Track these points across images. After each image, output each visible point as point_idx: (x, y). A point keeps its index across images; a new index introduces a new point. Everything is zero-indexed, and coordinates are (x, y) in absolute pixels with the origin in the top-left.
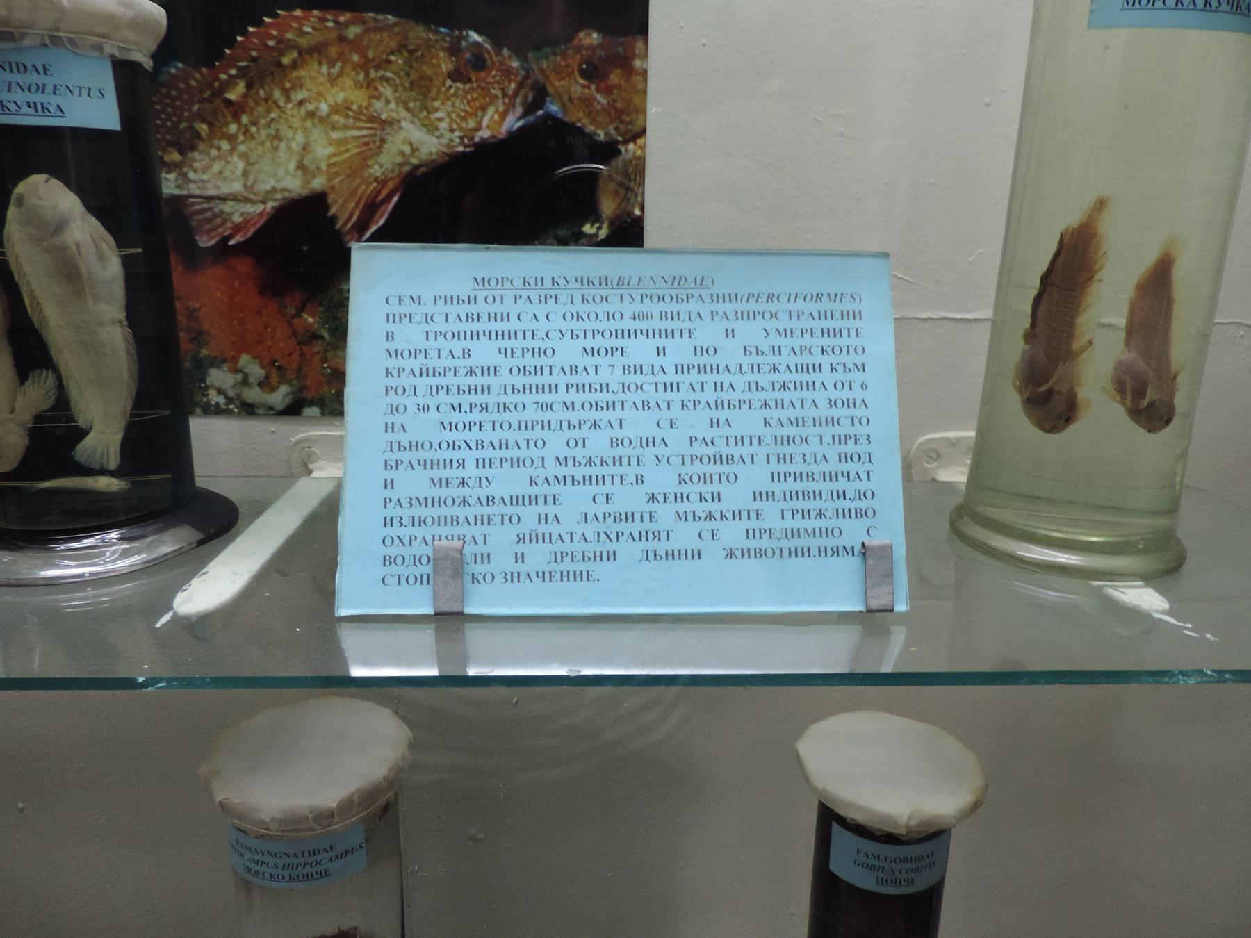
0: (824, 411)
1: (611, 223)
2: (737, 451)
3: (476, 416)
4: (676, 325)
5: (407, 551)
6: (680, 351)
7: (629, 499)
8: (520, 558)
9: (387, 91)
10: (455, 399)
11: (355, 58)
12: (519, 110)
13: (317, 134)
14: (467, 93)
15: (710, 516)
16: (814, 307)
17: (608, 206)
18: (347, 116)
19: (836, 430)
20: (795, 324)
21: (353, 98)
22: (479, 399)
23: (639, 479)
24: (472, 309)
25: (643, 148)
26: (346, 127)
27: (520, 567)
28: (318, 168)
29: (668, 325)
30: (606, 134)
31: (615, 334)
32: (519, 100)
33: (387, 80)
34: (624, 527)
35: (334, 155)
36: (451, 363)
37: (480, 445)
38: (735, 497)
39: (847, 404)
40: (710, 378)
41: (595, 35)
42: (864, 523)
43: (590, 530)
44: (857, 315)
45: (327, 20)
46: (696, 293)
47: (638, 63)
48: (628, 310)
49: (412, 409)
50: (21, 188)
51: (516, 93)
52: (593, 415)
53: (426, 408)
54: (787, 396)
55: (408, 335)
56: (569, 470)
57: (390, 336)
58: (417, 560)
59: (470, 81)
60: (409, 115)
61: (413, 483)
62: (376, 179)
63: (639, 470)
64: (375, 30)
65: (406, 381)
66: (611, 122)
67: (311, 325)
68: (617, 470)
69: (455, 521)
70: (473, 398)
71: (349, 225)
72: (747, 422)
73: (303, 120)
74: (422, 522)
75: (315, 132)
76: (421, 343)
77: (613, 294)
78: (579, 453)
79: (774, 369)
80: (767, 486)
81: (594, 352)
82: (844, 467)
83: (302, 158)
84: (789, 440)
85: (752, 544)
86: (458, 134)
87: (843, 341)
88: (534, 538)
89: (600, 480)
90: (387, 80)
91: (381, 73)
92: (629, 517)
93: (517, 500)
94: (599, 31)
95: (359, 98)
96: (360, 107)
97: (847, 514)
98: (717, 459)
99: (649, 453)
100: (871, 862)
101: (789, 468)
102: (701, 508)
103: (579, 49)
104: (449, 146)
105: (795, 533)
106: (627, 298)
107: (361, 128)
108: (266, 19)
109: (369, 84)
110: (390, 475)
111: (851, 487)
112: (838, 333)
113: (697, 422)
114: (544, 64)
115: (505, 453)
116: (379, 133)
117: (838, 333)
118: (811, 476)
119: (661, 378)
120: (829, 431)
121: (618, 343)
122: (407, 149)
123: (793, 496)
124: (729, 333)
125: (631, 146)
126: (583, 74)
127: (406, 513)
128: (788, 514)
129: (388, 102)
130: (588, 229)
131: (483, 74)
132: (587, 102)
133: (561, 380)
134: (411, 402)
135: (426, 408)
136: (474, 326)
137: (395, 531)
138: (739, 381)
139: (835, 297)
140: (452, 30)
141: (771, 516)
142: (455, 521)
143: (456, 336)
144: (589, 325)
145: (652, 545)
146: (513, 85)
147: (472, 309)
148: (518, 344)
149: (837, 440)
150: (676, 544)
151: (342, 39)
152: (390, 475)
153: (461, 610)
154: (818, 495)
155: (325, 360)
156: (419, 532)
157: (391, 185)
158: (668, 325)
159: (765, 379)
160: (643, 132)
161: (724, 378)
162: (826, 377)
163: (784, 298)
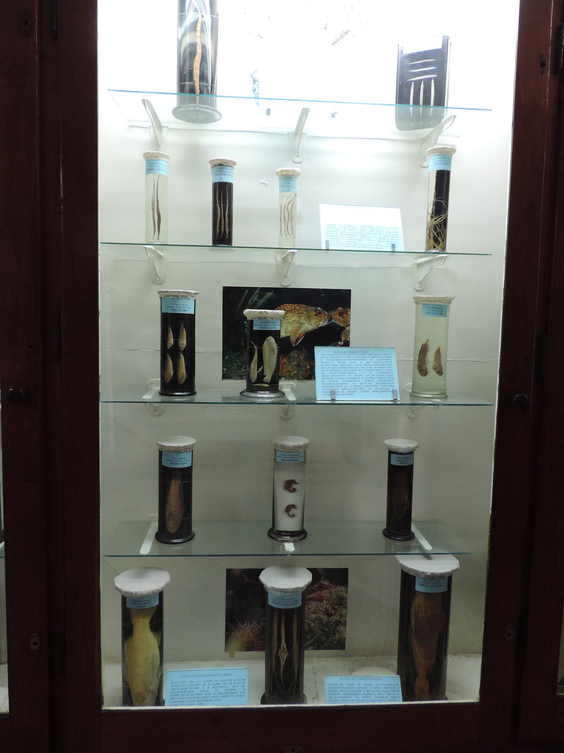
0: (386, 371)
1: (344, 342)
2: (373, 377)
3: (335, 372)
4: (363, 358)
5: (327, 391)
6: (364, 362)
7: (358, 384)
8: (343, 392)
9: (303, 318)
10: (332, 369)
11: (297, 312)
12: (327, 321)
13: (289, 326)
14: (317, 318)
15: (370, 386)
16: (384, 356)
17: (343, 339)
18: (295, 322)
19: (388, 374)
20: (381, 358)
21: (296, 319)
22: (336, 369)
23: (359, 381)
24: (333, 356)
25: (350, 328)
26: (294, 324)
27: (343, 393)
28: (289, 332)
29: (362, 358)
30: (343, 325)
31: (354, 360)
32: (327, 319)
33: (303, 316)
34: (358, 388)
35: (292, 329)
36: (331, 364)
37: (336, 376)
38: (373, 383)
39: (390, 370)
40: (369, 366)
41: (341, 308)
42: (393, 387)
43: (353, 388)
44: (390, 357)
45: (292, 306)
46: (366, 354)
47: (349, 313)
48: (356, 356)
49: (325, 371)
50: (268, 338)
51: (327, 318)
52: (352, 371)
53: (328, 370)
54: (381, 369)
55: (324, 360)
56: (349, 379)
57: (321, 360)
58: (328, 392)
59: (318, 316)
60: (307, 322)
61: (326, 381)
62: (299, 334)
63: (359, 380)
64: (301, 307)
65: (324, 366)
66: (344, 323)
67: (285, 361)
68: (356, 379)
69: (333, 386)
70: (334, 369)
71: (294, 342)
72: (375, 373)
73: (287, 323)
74: (328, 387)
75: (289, 325)
76: (326, 361)
77: (354, 354)
78: (350, 377)
79: (378, 365)
80: (378, 382)
81: (352, 362)
82: (389, 379)
83: (286, 330)
84: (381, 375)
85: (376, 390)
86: (315, 325)
87: (388, 361)
88: (345, 389)
89: (354, 381)
90: (303, 316)
91: (302, 315)
92: (358, 386)
93: (342, 384)
94: (342, 307)
95: (297, 319)
96: (297, 321)
97: (390, 386)
98: (371, 378)
99: (360, 377)
100: (399, 459)
101: (381, 379)
102: (369, 385)
103: (338, 310)
104: (314, 328)
105: (383, 389)
106: (356, 355)
107: (297, 325)
108: (282, 306)
109: (299, 317)
110: (323, 380)
111: (391, 382)
112: (388, 360)
113: (367, 373)
114: (332, 313)
115: (340, 377)
116: (301, 325)
117: (388, 360)
118: (385, 381)
119: (361, 366)
120: (387, 374)
121: (355, 361)
122: (306, 328)
123: (382, 383)
124: (371, 360)
125: (347, 327)
126: (339, 315)
127: (326, 385)
128: (381, 386)
129: (303, 320)
130: (339, 343)
131: (320, 315)
132: (340, 320)
133: (347, 367)
134: (325, 370)
135: (328, 370)
136: (334, 359)
137: (324, 388)
138: (373, 367)
139: (387, 354)
140: (315, 307)
141: (379, 386)
142: (333, 386)
143: (331, 360)
144: (350, 358)
145: (362, 390)
146: (326, 317)
147: (333, 356)
148: (340, 361)
149: (388, 375)
150: (365, 390)
151: (295, 309)
152: (323, 380)
153: (334, 399)
154: (386, 383)
155: (287, 368)
156: (328, 388)
157: (302, 335)
158: (362, 358)
159: (377, 366)
160: (350, 325)
161: (371, 366)
162: (386, 366)
163: (379, 354)
